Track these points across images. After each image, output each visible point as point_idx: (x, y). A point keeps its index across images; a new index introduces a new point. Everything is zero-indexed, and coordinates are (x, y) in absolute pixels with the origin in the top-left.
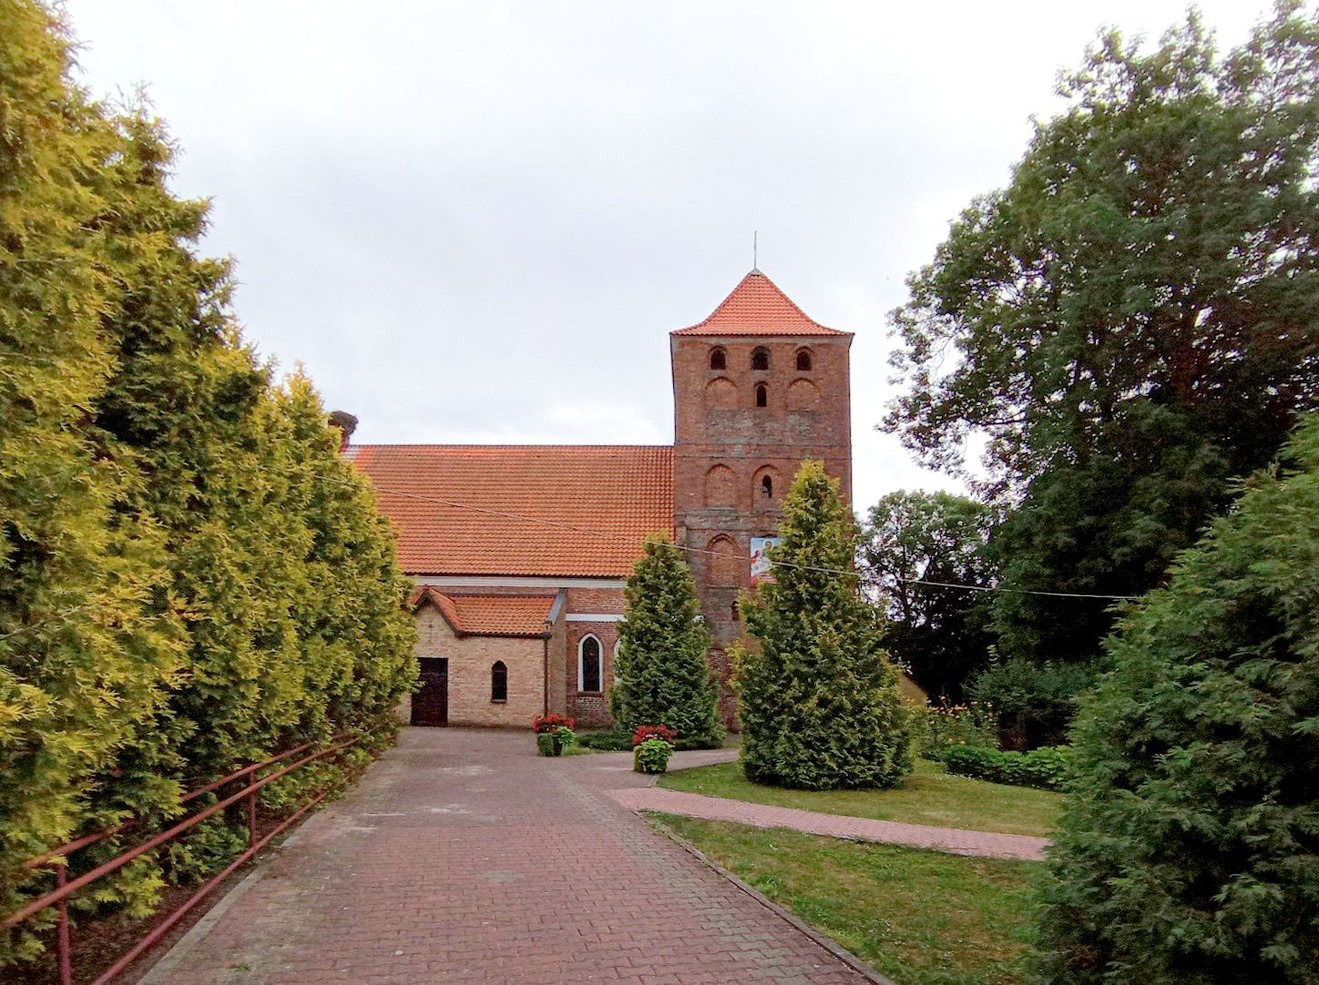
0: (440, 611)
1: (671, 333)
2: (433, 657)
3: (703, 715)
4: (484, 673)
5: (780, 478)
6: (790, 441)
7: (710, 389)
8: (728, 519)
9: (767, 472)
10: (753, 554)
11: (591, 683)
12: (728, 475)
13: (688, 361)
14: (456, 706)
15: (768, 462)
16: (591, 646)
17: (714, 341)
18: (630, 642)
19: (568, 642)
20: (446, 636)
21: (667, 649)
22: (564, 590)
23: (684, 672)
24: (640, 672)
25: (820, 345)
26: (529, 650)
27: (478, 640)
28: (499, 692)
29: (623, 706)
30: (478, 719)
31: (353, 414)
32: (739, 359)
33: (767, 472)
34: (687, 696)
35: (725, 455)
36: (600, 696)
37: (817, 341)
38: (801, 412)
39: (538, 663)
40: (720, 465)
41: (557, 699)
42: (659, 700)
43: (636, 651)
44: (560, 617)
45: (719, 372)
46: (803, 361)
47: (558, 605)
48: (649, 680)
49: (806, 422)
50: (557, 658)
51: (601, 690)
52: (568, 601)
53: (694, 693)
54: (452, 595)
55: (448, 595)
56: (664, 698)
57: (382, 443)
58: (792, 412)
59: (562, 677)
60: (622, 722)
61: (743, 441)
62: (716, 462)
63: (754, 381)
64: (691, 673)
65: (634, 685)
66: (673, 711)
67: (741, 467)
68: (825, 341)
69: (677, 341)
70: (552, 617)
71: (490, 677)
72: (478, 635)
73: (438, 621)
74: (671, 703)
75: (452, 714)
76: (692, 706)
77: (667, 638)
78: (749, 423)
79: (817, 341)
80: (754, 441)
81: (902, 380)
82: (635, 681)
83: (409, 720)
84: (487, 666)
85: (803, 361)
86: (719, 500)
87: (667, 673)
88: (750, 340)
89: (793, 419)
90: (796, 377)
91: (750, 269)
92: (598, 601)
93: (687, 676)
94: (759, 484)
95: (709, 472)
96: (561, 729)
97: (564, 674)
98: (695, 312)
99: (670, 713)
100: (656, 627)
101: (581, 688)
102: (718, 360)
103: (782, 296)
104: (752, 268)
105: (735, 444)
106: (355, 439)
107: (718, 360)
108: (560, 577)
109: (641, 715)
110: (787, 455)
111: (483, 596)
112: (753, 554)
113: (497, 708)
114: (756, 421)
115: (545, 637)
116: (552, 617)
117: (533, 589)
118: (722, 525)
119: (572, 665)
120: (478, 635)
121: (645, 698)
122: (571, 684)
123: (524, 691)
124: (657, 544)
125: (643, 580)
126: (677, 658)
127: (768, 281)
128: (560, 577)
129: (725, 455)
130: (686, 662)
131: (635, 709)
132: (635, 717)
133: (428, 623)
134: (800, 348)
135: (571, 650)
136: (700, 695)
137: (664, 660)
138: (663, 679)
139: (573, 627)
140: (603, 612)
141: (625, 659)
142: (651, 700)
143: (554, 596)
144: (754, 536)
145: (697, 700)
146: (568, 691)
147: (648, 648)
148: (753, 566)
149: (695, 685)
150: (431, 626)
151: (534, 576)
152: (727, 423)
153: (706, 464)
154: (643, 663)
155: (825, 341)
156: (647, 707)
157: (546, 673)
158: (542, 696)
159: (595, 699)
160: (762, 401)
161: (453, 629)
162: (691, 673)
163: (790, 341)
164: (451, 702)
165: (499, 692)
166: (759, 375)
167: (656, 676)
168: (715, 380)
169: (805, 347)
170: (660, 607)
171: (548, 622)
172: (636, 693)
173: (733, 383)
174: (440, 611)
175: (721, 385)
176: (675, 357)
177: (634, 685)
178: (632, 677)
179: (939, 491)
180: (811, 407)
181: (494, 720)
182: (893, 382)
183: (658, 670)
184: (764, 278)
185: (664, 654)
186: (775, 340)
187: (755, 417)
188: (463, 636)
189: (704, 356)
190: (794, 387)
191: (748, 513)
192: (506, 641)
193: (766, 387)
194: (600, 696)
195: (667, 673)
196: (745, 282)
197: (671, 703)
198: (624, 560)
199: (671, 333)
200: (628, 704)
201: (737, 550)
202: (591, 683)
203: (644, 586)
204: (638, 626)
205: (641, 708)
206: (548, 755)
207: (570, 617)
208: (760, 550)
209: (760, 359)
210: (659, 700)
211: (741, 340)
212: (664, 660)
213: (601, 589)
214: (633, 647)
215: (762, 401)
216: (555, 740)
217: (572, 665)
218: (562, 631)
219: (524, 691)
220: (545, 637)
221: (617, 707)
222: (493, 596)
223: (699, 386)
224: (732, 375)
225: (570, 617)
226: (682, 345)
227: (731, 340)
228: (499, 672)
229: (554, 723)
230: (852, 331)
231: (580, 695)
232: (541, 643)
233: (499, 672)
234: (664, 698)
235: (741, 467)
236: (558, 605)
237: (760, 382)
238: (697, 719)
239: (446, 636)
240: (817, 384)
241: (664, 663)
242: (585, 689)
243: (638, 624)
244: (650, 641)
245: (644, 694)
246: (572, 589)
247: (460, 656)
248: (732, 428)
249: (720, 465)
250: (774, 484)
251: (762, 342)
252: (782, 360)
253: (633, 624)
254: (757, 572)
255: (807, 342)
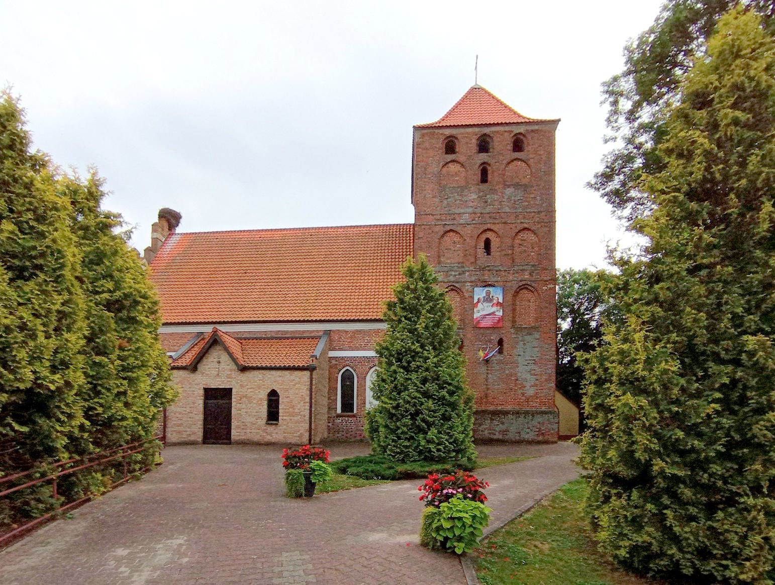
0: (226, 349)
1: (414, 127)
2: (220, 387)
3: (462, 436)
4: (261, 399)
5: (498, 240)
6: (508, 210)
7: (445, 169)
8: (457, 273)
9: (489, 235)
10: (475, 301)
11: (348, 406)
12: (456, 238)
13: (427, 149)
14: (238, 427)
15: (489, 226)
16: (348, 379)
17: (448, 132)
18: (390, 364)
19: (330, 373)
20: (231, 370)
21: (427, 370)
22: (328, 333)
23: (444, 393)
24: (399, 393)
25: (532, 131)
26: (297, 380)
27: (256, 373)
28: (273, 415)
29: (381, 429)
30: (256, 438)
31: (178, 211)
32: (467, 146)
33: (489, 235)
34: (446, 418)
35: (455, 222)
36: (354, 416)
37: (530, 128)
38: (517, 186)
39: (305, 392)
40: (451, 231)
41: (321, 420)
42: (419, 422)
43: (395, 372)
44: (324, 353)
45: (450, 157)
46: (518, 145)
47: (321, 345)
48: (408, 402)
49: (520, 194)
50: (320, 386)
51: (355, 411)
52: (331, 341)
53: (453, 414)
54: (241, 339)
55: (237, 339)
56: (423, 420)
57: (197, 231)
58: (509, 186)
59: (325, 401)
60: (379, 446)
61: (470, 210)
62: (448, 228)
63: (479, 162)
64: (451, 393)
65: (394, 408)
66: (432, 433)
67: (467, 231)
68: (536, 127)
69: (418, 133)
70: (317, 353)
71: (265, 403)
72: (257, 368)
73: (225, 357)
74: (429, 425)
75: (235, 434)
76: (451, 428)
77: (429, 358)
78: (474, 196)
79: (530, 128)
80: (478, 210)
81: (616, 138)
82: (395, 403)
83: (200, 439)
84: (263, 395)
85: (518, 145)
86: (448, 258)
87: (426, 395)
88: (476, 130)
89: (509, 191)
90: (513, 158)
91: (472, 84)
92: (354, 342)
93: (447, 397)
94: (482, 245)
95: (443, 236)
96: (315, 463)
97: (326, 399)
98: (433, 117)
99: (430, 435)
100: (416, 347)
101: (339, 411)
102: (450, 147)
103: (498, 101)
104: (474, 84)
105: (464, 213)
106: (179, 230)
107: (450, 147)
108: (324, 321)
109: (399, 438)
110: (503, 221)
111: (264, 339)
112: (475, 301)
113: (271, 429)
114: (481, 194)
115: (311, 369)
116: (317, 353)
117: (304, 332)
118: (452, 278)
119: (332, 390)
120: (257, 368)
121: (404, 420)
122: (331, 407)
123: (293, 415)
124: (416, 267)
125: (402, 301)
126: (438, 378)
127: (486, 92)
128: (324, 321)
129: (455, 222)
130: (446, 382)
131: (393, 431)
132: (393, 441)
133: (217, 360)
134: (516, 134)
135: (332, 380)
136: (458, 415)
137: (424, 381)
138: (423, 400)
139: (334, 362)
140: (357, 349)
141: (384, 380)
142: (410, 422)
143: (320, 337)
144: (477, 286)
145: (456, 421)
146: (328, 413)
147: (407, 369)
148: (475, 310)
149: (453, 406)
150: (219, 362)
151: (304, 321)
152: (457, 197)
153: (440, 230)
154: (402, 385)
155: (536, 127)
156: (405, 429)
157: (311, 398)
158: (308, 416)
159: (350, 419)
160: (484, 179)
161: (236, 364)
162: (451, 393)
163: (507, 128)
164: (234, 423)
165: (273, 415)
166: (483, 157)
167: (415, 398)
168: (447, 163)
169: (520, 134)
170: (420, 327)
171: (312, 356)
172: (394, 415)
173: (463, 166)
174: (226, 349)
175: (453, 168)
176: (416, 146)
177: (394, 408)
178: (391, 399)
179: (581, 270)
180: (524, 181)
181: (268, 438)
182: (606, 141)
183: (418, 391)
184: (483, 89)
185: (424, 374)
186: (494, 129)
187: (480, 191)
188: (244, 369)
189: (440, 144)
190: (510, 166)
191: (471, 268)
192: (279, 373)
193: (489, 168)
194: (354, 416)
195: (426, 395)
196: (469, 93)
197: (429, 425)
198: (375, 307)
199: (414, 127)
200: (386, 426)
201: (463, 298)
202: (348, 406)
203: (404, 309)
204: (399, 347)
205: (399, 431)
206: (298, 496)
207: (332, 354)
208: (481, 297)
209: (484, 146)
210: (419, 422)
211: (470, 130)
212: (424, 381)
213: (357, 331)
214: (393, 368)
215: (484, 179)
216: (307, 478)
217: (332, 390)
218: (325, 365)
219: (293, 415)
220: (311, 369)
221: (374, 430)
222: (272, 338)
223: (434, 168)
224: (462, 159)
225: (332, 354)
226: (423, 136)
227: (462, 130)
228: (273, 398)
229: (307, 456)
230: (557, 118)
231: (338, 416)
232: (307, 373)
233: (273, 398)
234: (423, 420)
235: (467, 231)
236: (321, 345)
237: (484, 163)
238: (455, 441)
239: (231, 370)
240: (529, 162)
241: (424, 384)
242: (343, 411)
243: (398, 345)
244: (409, 362)
245: (403, 416)
246: (334, 331)
247: (242, 386)
248: (461, 200)
249: (451, 231)
250: (492, 244)
251: (486, 130)
252: (501, 144)
253: (392, 345)
254: (479, 315)
255: (522, 129)
